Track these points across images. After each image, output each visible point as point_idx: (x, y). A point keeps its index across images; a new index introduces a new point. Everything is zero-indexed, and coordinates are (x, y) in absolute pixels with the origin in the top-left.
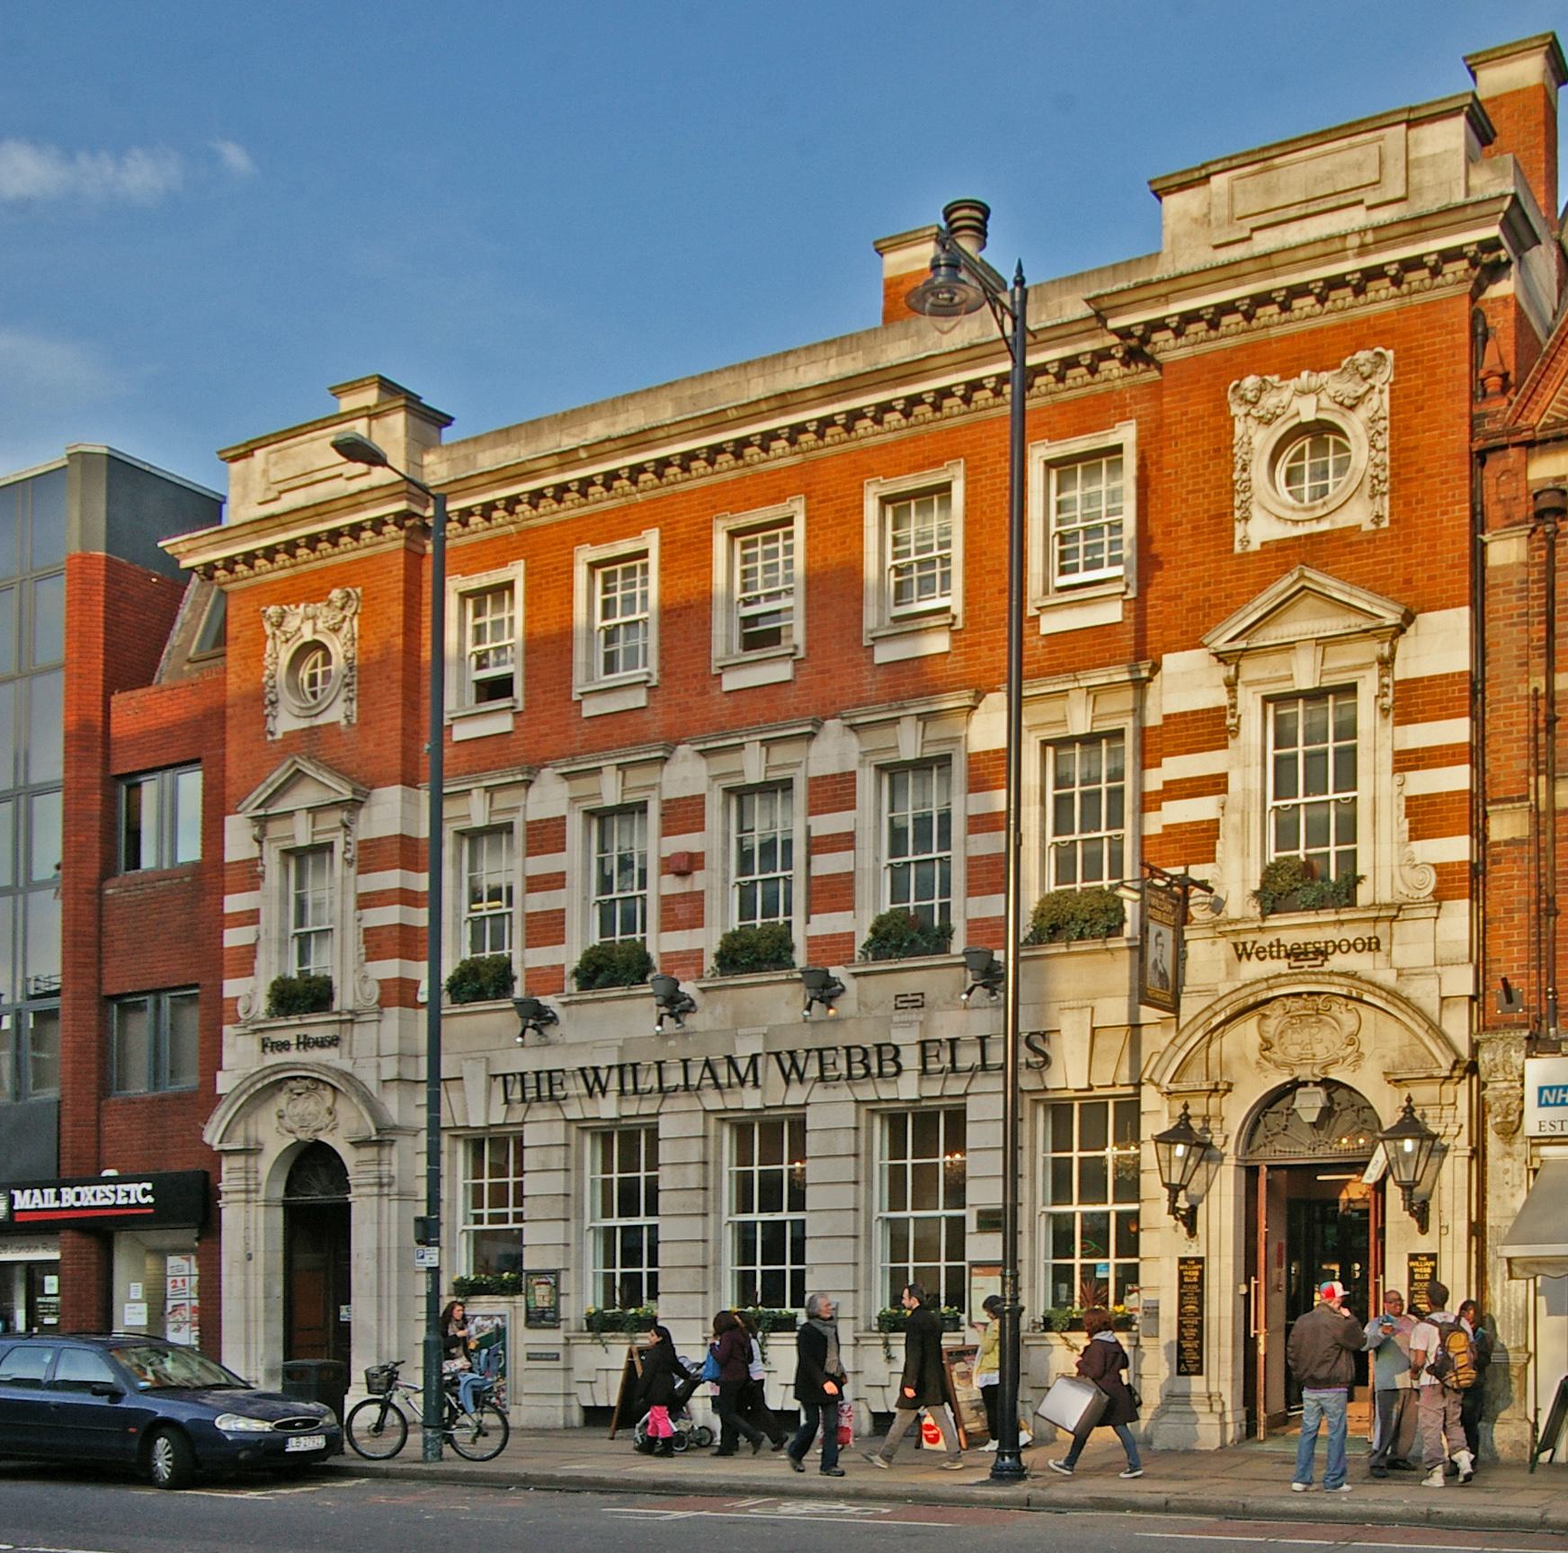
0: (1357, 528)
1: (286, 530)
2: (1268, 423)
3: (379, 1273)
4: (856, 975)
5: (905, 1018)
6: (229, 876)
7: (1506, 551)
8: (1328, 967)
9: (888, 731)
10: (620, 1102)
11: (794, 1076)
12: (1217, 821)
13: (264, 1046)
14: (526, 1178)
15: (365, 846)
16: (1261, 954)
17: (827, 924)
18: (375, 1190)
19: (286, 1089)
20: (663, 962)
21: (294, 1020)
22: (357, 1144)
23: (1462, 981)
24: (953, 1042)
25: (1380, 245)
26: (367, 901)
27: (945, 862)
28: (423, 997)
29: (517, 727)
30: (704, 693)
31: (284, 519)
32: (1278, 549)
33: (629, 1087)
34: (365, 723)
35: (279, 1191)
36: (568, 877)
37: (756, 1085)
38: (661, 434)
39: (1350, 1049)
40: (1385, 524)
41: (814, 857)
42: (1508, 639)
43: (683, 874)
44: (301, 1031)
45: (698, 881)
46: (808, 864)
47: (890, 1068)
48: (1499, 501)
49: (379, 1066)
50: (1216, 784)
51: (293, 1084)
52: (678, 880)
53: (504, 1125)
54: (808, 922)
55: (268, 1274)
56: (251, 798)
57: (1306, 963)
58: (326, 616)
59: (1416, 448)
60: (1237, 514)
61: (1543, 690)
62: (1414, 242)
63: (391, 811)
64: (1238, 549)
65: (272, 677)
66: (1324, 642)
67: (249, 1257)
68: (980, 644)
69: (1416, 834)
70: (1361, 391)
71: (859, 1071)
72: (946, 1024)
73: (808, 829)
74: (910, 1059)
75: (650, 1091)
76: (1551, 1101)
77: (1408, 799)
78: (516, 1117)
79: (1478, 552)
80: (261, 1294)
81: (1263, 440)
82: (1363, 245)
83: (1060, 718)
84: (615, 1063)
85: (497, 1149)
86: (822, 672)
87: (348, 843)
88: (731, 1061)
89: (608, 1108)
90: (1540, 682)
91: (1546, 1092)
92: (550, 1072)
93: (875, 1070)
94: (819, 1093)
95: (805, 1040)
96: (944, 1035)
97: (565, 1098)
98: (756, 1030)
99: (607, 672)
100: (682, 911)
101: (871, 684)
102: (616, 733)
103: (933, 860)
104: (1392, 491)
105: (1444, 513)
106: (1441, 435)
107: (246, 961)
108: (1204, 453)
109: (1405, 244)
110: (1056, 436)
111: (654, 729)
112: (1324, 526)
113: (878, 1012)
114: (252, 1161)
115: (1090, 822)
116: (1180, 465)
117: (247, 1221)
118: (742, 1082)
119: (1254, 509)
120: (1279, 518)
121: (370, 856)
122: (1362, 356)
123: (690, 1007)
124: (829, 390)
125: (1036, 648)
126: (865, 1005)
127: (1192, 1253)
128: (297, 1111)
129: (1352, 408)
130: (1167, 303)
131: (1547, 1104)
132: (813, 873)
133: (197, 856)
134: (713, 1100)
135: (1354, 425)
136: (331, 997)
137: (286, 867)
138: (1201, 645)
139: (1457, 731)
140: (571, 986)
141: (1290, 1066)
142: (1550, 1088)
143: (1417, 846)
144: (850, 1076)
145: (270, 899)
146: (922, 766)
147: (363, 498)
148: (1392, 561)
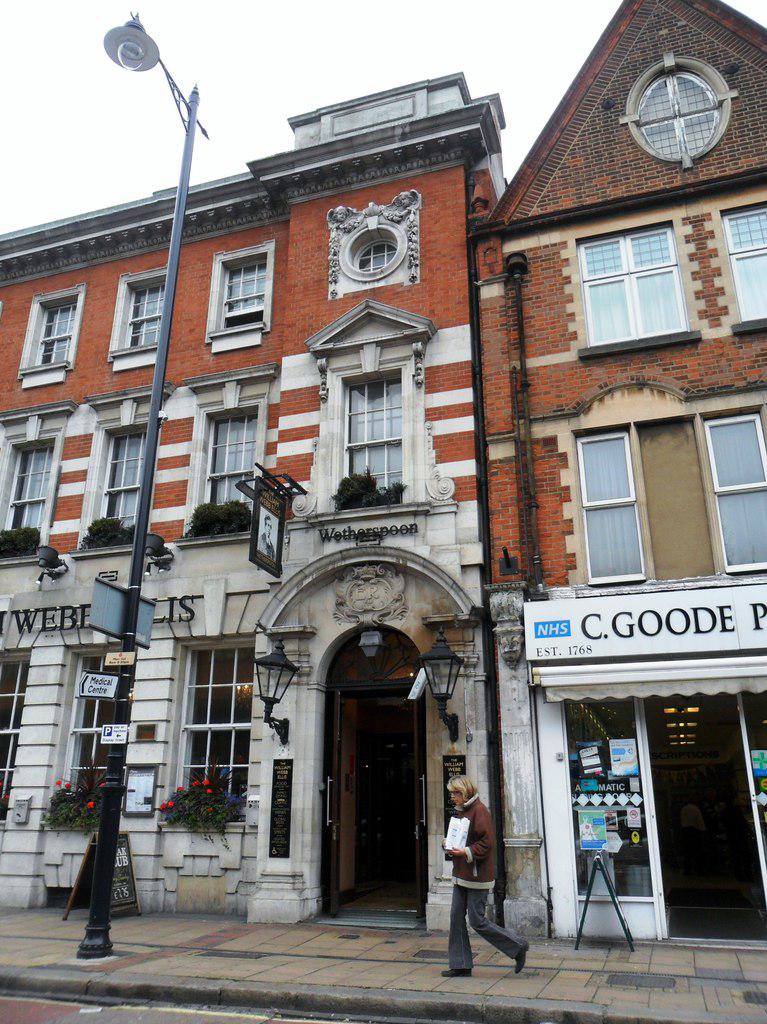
0: (401, 285)
7: (491, 292)
12: (312, 454)
16: (338, 537)
26: (433, 414)
42: (496, 338)
59: (435, 242)
64: (330, 297)
69: (441, 459)
73: (60, 468)
76: (545, 633)
81: (347, 241)
90: (517, 364)
91: (541, 627)
112: (382, 284)
120: (355, 280)
129: (398, 222)
131: (542, 636)
142: (544, 624)
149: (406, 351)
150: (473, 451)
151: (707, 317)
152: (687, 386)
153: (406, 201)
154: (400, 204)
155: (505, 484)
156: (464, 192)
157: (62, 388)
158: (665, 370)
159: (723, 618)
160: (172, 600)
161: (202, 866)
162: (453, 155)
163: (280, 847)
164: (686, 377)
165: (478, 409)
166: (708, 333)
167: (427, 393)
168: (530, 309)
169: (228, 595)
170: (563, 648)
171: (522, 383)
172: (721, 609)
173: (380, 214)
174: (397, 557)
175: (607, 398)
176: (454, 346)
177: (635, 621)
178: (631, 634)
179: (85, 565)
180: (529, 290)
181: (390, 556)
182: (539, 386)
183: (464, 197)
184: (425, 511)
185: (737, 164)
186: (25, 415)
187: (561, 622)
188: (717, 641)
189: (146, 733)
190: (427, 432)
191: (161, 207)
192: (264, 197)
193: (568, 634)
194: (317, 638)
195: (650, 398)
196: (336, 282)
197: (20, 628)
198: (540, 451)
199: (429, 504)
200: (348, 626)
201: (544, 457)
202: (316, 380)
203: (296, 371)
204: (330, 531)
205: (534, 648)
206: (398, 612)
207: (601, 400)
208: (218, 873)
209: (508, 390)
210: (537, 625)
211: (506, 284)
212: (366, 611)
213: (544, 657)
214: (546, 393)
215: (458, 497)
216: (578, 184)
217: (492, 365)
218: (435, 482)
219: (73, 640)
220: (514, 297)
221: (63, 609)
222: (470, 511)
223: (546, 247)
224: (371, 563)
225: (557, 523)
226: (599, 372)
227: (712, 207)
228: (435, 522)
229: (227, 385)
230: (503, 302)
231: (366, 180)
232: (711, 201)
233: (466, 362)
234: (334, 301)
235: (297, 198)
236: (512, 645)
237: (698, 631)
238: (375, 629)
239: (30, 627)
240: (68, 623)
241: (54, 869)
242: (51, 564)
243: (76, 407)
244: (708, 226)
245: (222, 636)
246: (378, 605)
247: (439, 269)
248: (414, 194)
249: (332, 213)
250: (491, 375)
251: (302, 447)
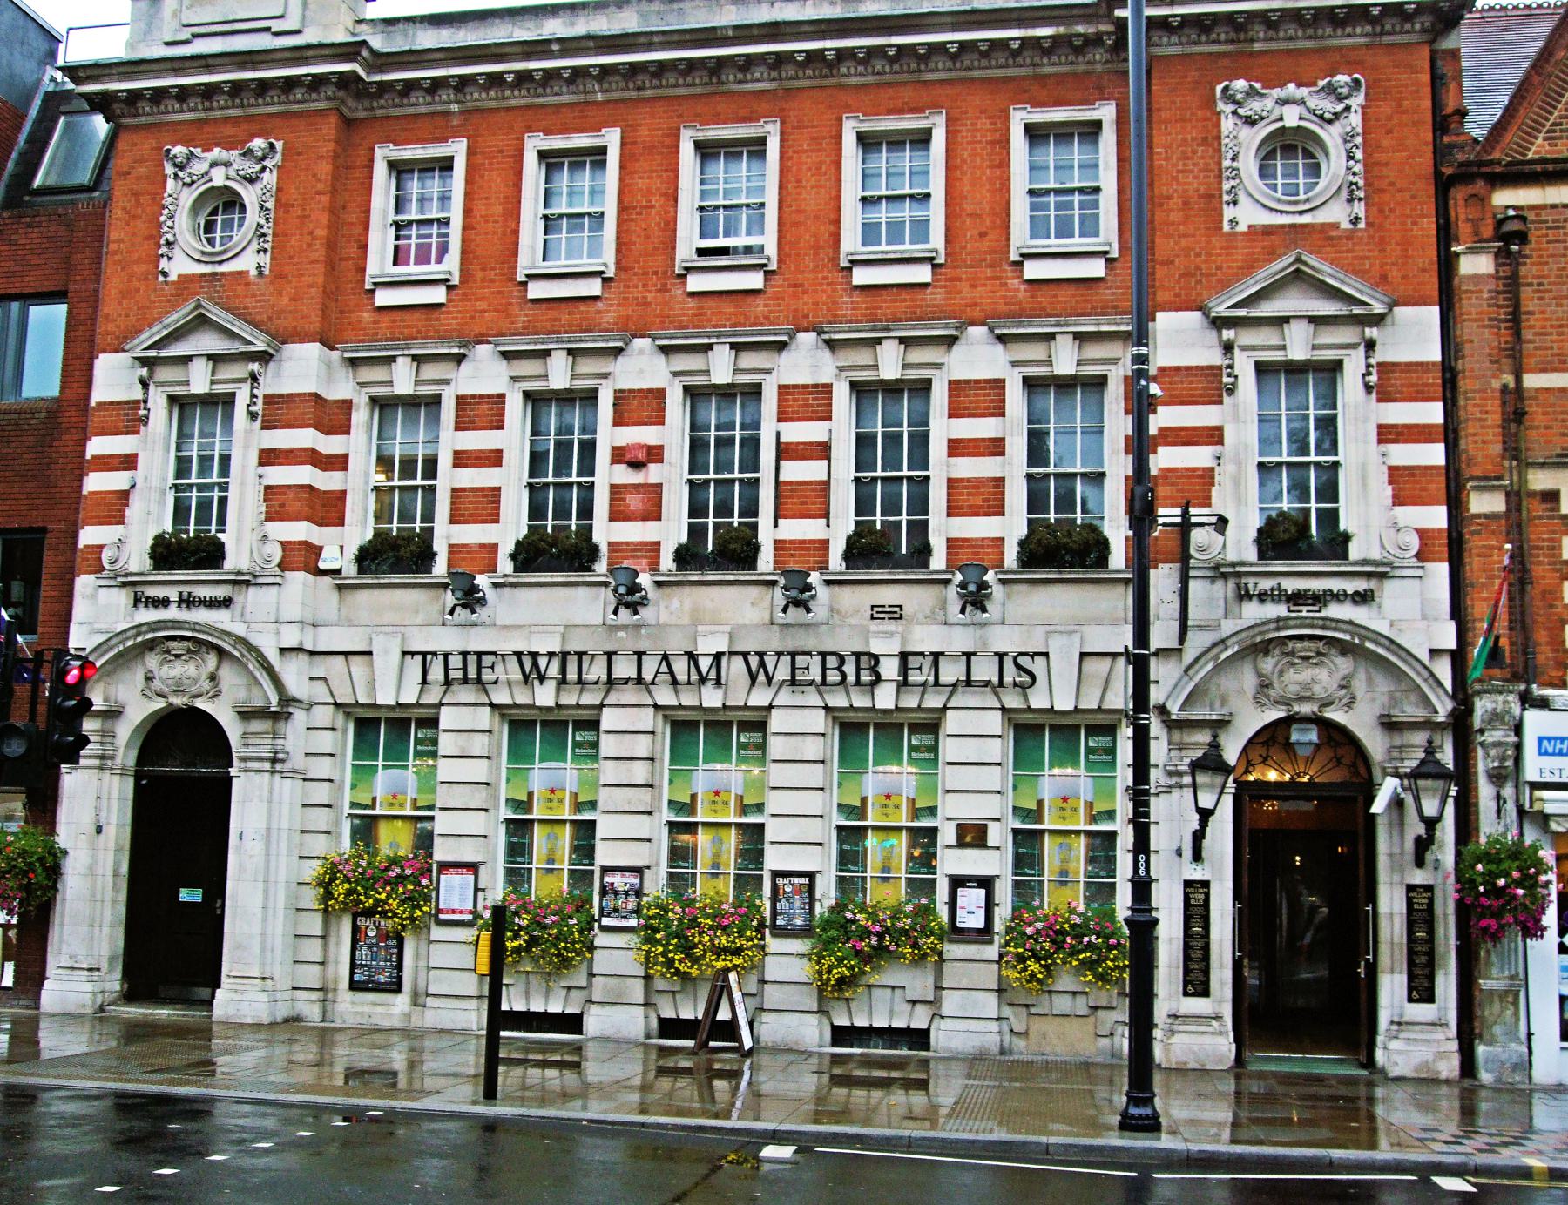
0: (1335, 226)
1: (211, 73)
3: (268, 854)
4: (828, 583)
5: (881, 628)
6: (95, 420)
7: (1475, 265)
10: (558, 690)
11: (762, 678)
12: (1212, 469)
13: (137, 601)
15: (270, 400)
16: (1263, 597)
17: (472, 534)
18: (267, 766)
20: (610, 551)
21: (180, 575)
24: (937, 656)
27: (430, 492)
28: (1118, 558)
29: (449, 300)
30: (664, 290)
31: (211, 62)
33: (572, 675)
34: (278, 275)
35: (131, 761)
36: (505, 455)
37: (718, 682)
39: (1343, 692)
40: (1362, 225)
41: (783, 463)
42: (1479, 338)
43: (636, 465)
44: (186, 589)
45: (653, 473)
48: (1468, 220)
49: (278, 633)
50: (1213, 436)
52: (630, 471)
53: (418, 705)
54: (776, 526)
55: (118, 850)
56: (143, 337)
57: (1305, 608)
59: (1387, 164)
60: (1226, 198)
61: (1512, 385)
63: (304, 368)
64: (1226, 227)
65: (171, 217)
66: (215, 359)
67: (99, 830)
68: (960, 279)
69: (1398, 500)
71: (833, 677)
72: (925, 639)
74: (890, 669)
75: (596, 683)
76: (1550, 750)
78: (431, 698)
80: (110, 873)
81: (188, 197)
83: (1044, 357)
84: (557, 650)
86: (795, 286)
87: (253, 396)
88: (692, 657)
90: (1509, 379)
91: (1545, 743)
92: (479, 654)
93: (851, 678)
94: (785, 697)
95: (773, 642)
96: (927, 648)
97: (496, 682)
98: (721, 628)
99: (395, 263)
100: (634, 502)
102: (887, 309)
103: (900, 479)
104: (1367, 197)
105: (1415, 223)
106: (1410, 157)
107: (115, 508)
108: (1193, 139)
110: (1037, 103)
111: (610, 317)
113: (853, 621)
114: (109, 724)
115: (562, 467)
116: (1170, 146)
117: (99, 789)
119: (1242, 197)
120: (1264, 206)
121: (277, 411)
122: (1342, 79)
123: (482, 601)
125: (1018, 290)
126: (839, 612)
128: (172, 674)
129: (1330, 122)
131: (1546, 753)
132: (782, 478)
133: (54, 390)
134: (665, 697)
135: (1331, 136)
136: (223, 557)
137: (372, 411)
140: (505, 566)
141: (1286, 702)
142: (1549, 739)
143: (1400, 511)
144: (824, 682)
145: (155, 445)
146: (412, 403)
147: (310, 53)
148: (1368, 258)
149: (1347, 335)
150: (1443, 495)
153: (1345, 91)
154: (1331, 90)
156: (1428, 89)
160: (1001, 656)
162: (1418, 26)
165: (1450, 434)
167: (1379, 400)
168: (1529, 300)
169: (1083, 655)
171: (1515, 407)
173: (1302, 102)
174: (1352, 634)
176: (1415, 335)
179: (845, 593)
180: (1527, 270)
181: (1344, 632)
182: (1536, 414)
183: (1429, 95)
184: (1380, 572)
186: (706, 341)
190: (1381, 459)
191: (929, 21)
192: (1108, 34)
194: (1231, 728)
196: (1235, 203)
197: (753, 679)
198: (1538, 509)
199: (1390, 564)
201: (1540, 517)
204: (1251, 587)
205: (1534, 767)
206: (1345, 701)
209: (1498, 417)
210: (1540, 740)
211: (1497, 255)
212: (1302, 699)
213: (1548, 778)
214: (1547, 428)
217: (1477, 377)
218: (1393, 531)
219: (838, 700)
220: (1506, 278)
222: (1440, 572)
223: (1554, 206)
224: (1311, 638)
228: (1390, 586)
229: (1058, 337)
230: (1492, 285)
231: (1278, 39)
234: (1233, 235)
236: (1503, 759)
243: (792, 336)
246: (1318, 691)
247: (1391, 211)
248: (1357, 82)
249: (1226, 89)
250: (1474, 391)
251: (1198, 457)
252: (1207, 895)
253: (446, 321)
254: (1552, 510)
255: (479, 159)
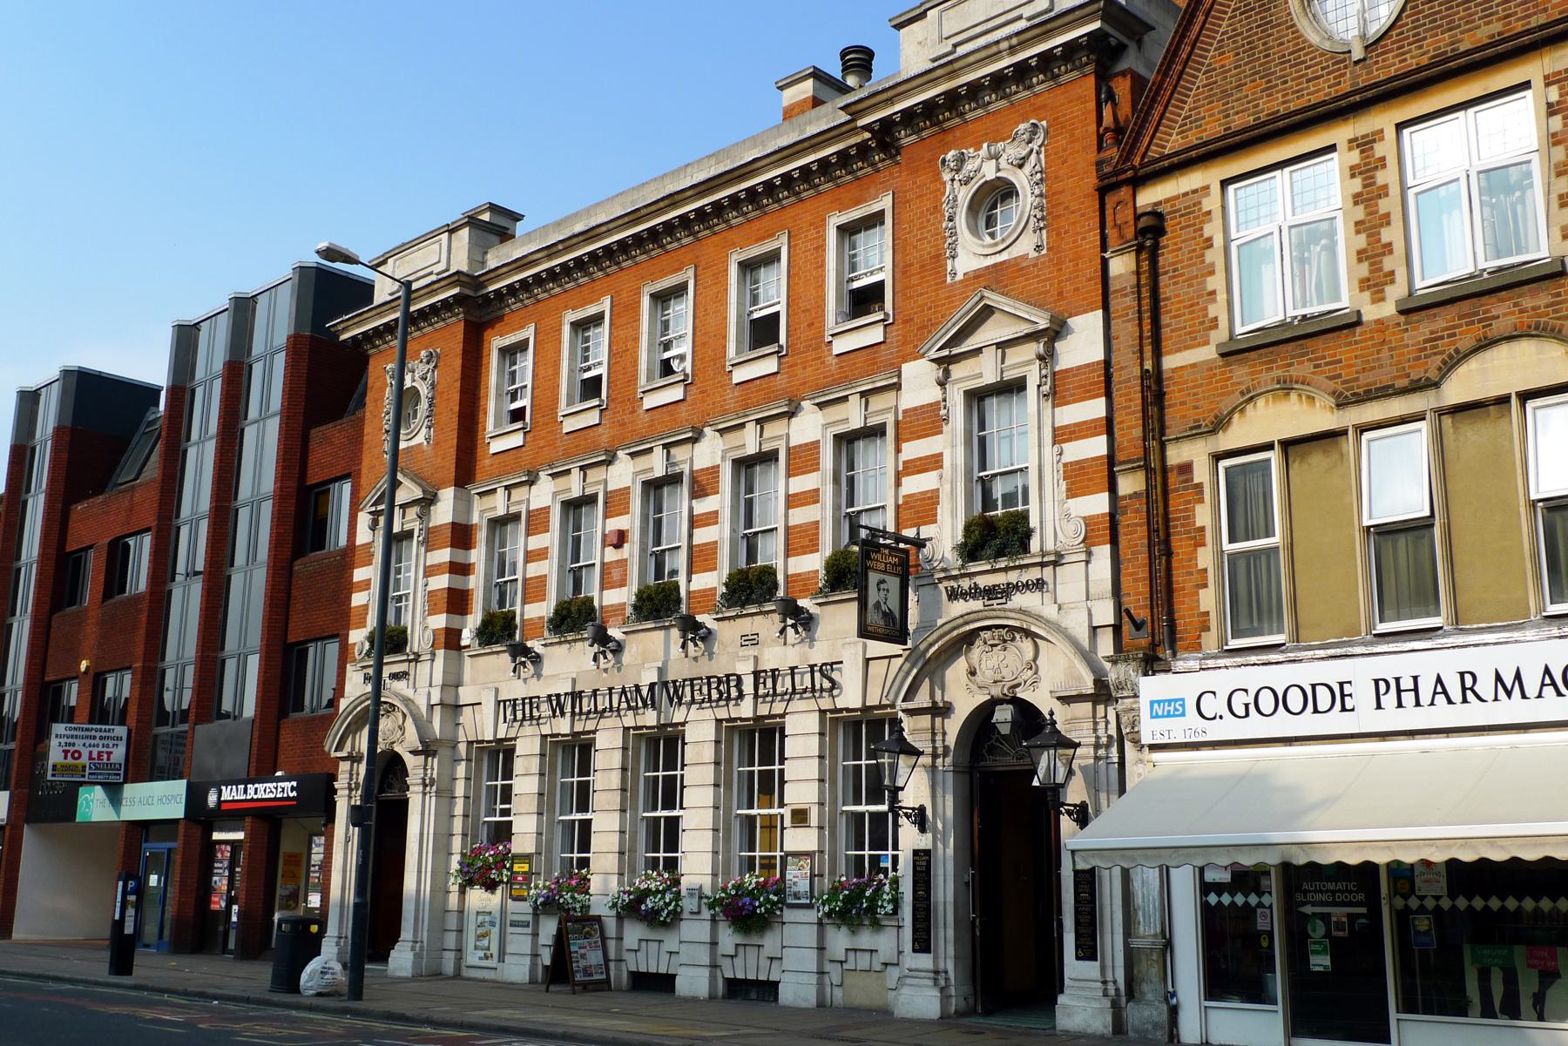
0: (1025, 257)
2: (1021, 166)
8: (1010, 605)
9: (738, 434)
14: (787, 766)
19: (978, 642)
22: (1066, 700)
23: (1105, 613)
25: (1024, 45)
26: (1062, 435)
30: (633, 412)
32: (976, 277)
38: (604, 229)
42: (1126, 331)
46: (787, 516)
47: (734, 693)
51: (985, 635)
58: (1013, 151)
62: (1045, 40)
69: (1072, 493)
70: (1024, 153)
73: (691, 509)
74: (748, 686)
77: (1065, 465)
79: (1105, 264)
81: (964, 195)
82: (1011, 47)
85: (500, 755)
88: (637, 687)
89: (563, 726)
101: (731, 397)
109: (1040, 42)
112: (1004, 257)
118: (645, 705)
124: (702, 188)
127: (922, 846)
130: (893, 104)
131: (1157, 716)
138: (923, 356)
139: (1095, 408)
142: (1159, 702)
151: (1369, 288)
152: (1340, 388)
155: (1136, 525)
157: (683, 407)
158: (1316, 366)
159: (1343, 696)
160: (812, 667)
161: (863, 961)
163: (922, 943)
164: (1340, 376)
166: (1371, 313)
168: (1167, 288)
170: (1178, 730)
172: (1341, 684)
175: (1249, 407)
176: (1084, 344)
177: (1251, 700)
178: (1247, 715)
180: (1165, 259)
185: (1421, 47)
187: (1176, 700)
188: (1335, 722)
189: (800, 817)
193: (1183, 714)
195: (1297, 407)
197: (671, 700)
200: (983, 698)
202: (934, 394)
203: (918, 383)
207: (1242, 411)
208: (878, 967)
215: (1088, 542)
216: (1226, 94)
221: (709, 678)
222: (1103, 553)
223: (1186, 194)
225: (1191, 574)
226: (1240, 373)
227: (1382, 120)
232: (1346, 120)
233: (1098, 363)
235: (906, 139)
237: (1316, 711)
238: (1008, 702)
239: (680, 699)
240: (715, 695)
241: (729, 960)
242: (691, 628)
244: (1379, 150)
245: (866, 709)
246: (1007, 674)
252: (929, 862)
253: (525, 457)
254: (1186, 481)
255: (541, 337)
